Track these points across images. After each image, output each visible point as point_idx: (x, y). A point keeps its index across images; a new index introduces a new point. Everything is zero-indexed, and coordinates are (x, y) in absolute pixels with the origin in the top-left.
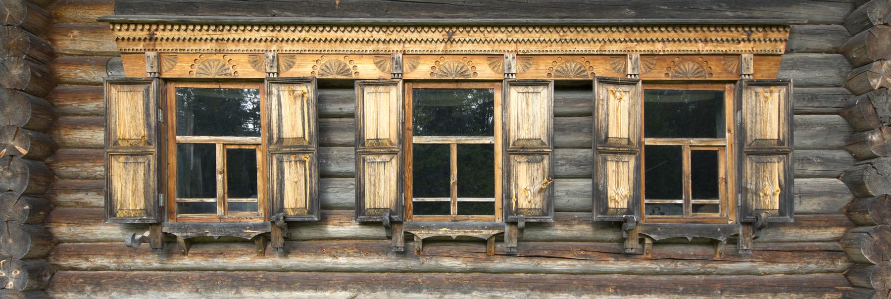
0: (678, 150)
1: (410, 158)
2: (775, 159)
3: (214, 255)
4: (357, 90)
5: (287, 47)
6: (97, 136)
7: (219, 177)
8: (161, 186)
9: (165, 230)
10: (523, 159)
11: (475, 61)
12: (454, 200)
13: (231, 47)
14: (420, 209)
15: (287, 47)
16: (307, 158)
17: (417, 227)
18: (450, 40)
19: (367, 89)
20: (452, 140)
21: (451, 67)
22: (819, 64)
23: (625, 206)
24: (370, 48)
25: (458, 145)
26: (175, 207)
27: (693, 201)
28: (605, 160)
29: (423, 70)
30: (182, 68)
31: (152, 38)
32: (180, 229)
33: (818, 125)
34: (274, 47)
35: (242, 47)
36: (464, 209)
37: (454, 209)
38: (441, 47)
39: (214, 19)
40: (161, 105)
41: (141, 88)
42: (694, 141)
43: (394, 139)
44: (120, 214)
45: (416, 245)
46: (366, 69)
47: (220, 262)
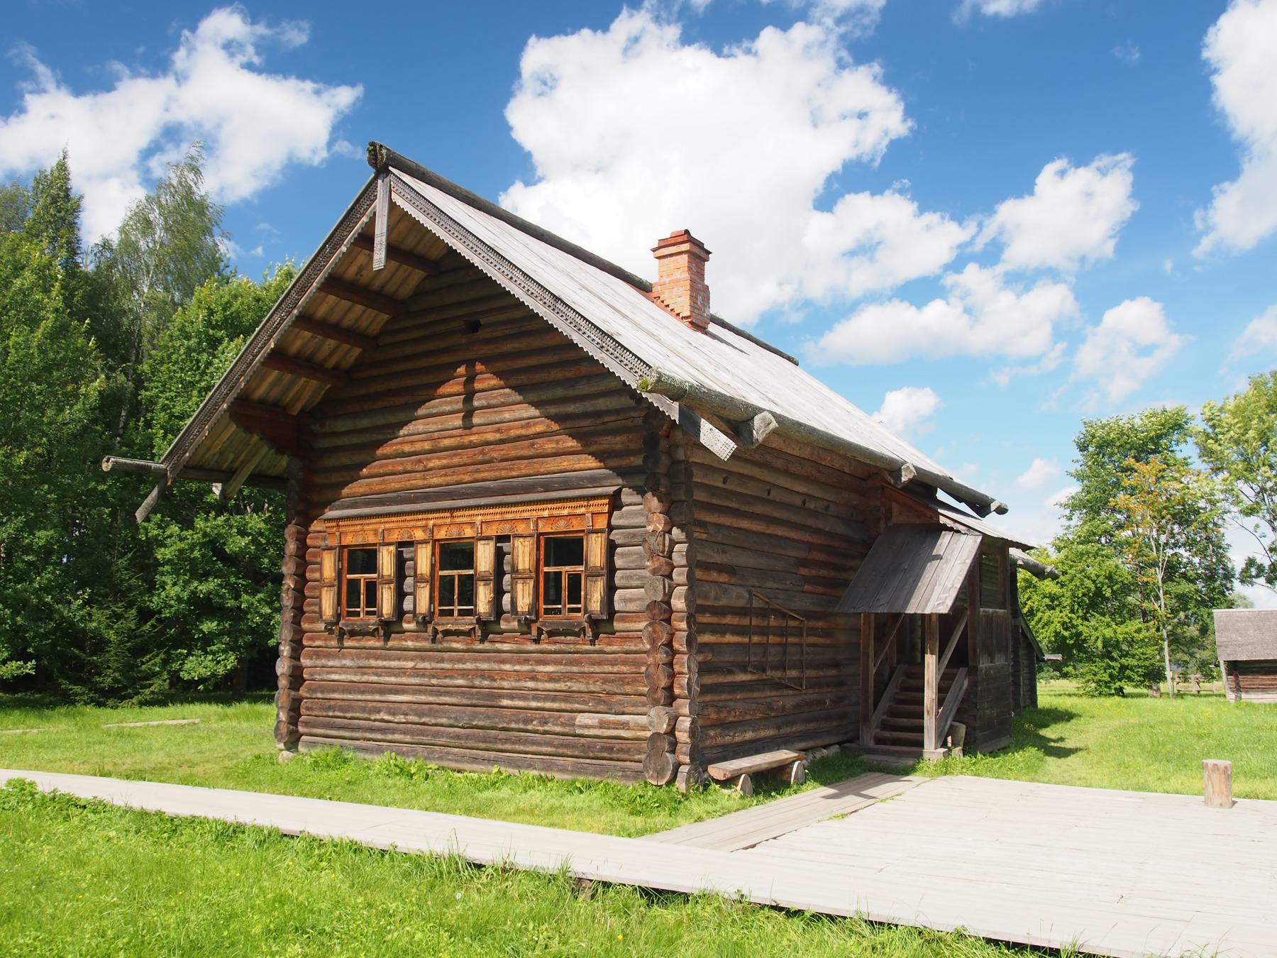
0: (358, 581)
1: (437, 584)
2: (599, 578)
3: (359, 640)
4: (415, 545)
5: (388, 526)
6: (317, 575)
7: (362, 596)
8: (339, 603)
9: (340, 626)
10: (482, 583)
11: (464, 526)
12: (456, 608)
13: (366, 527)
14: (442, 613)
15: (388, 526)
16: (392, 586)
17: (438, 624)
18: (452, 517)
19: (419, 546)
20: (455, 572)
21: (454, 532)
22: (636, 514)
23: (527, 610)
24: (420, 523)
25: (459, 576)
26: (345, 613)
27: (568, 606)
28: (517, 583)
29: (441, 534)
30: (348, 540)
31: (338, 526)
32: (346, 626)
33: (635, 554)
34: (382, 526)
35: (371, 527)
36: (462, 613)
37: (456, 613)
38: (448, 521)
39: (350, 792)
40: (340, 559)
41: (333, 551)
42: (567, 568)
43: (428, 574)
44: (324, 618)
45: (439, 636)
46: (419, 535)
47: (362, 643)
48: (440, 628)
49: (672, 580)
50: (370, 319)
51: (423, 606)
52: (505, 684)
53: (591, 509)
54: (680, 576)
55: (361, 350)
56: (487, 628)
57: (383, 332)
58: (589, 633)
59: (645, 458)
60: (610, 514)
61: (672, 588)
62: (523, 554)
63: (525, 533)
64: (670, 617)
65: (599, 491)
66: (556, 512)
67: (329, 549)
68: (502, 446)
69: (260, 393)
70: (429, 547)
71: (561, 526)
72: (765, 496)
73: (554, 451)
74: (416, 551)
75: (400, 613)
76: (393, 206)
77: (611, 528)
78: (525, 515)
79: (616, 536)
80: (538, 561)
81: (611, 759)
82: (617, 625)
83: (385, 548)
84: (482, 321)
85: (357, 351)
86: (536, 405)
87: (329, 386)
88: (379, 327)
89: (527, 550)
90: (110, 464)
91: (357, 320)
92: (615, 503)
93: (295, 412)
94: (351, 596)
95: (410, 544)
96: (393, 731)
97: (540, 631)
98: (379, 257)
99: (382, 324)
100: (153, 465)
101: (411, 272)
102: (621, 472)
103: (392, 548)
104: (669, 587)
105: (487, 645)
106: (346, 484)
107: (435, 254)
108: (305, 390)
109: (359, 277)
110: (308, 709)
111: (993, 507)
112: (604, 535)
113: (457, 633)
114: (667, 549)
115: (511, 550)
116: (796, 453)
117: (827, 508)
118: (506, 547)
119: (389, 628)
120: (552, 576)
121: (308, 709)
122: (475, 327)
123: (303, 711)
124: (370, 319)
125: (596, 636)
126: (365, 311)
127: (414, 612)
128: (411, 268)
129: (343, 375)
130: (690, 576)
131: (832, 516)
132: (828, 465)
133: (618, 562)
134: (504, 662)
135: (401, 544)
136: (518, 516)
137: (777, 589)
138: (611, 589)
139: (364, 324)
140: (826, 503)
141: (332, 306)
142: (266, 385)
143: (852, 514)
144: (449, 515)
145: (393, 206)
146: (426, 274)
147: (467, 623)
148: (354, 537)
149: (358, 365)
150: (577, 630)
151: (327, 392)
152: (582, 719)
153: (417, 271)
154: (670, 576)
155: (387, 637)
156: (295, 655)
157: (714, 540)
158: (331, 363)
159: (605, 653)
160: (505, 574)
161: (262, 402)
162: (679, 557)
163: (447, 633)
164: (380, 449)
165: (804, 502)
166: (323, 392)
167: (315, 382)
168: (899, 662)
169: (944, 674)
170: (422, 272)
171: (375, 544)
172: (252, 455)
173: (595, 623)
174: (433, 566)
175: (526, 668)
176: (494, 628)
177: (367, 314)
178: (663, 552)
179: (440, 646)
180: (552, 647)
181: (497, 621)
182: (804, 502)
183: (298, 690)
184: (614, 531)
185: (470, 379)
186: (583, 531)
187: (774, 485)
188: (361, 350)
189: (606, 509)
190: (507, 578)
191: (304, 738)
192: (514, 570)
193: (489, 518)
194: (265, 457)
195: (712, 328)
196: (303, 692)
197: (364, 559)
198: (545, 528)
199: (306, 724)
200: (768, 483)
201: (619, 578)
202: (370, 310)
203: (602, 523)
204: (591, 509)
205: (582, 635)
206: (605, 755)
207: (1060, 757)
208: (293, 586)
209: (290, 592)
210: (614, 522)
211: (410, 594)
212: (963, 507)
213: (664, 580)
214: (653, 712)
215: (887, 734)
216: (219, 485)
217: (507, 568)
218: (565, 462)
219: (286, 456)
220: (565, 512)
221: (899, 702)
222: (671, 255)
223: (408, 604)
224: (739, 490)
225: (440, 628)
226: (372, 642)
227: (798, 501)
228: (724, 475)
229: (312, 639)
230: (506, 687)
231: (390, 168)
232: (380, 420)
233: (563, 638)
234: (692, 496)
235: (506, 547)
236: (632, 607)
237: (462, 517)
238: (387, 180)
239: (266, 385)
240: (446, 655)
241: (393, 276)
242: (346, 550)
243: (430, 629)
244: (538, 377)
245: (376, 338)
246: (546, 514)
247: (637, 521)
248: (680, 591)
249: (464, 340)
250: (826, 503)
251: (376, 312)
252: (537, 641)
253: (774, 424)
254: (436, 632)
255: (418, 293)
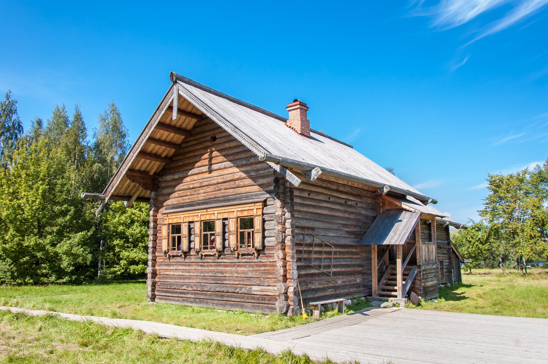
6: (160, 235)
30: (171, 221)
31: (168, 216)
38: (206, 213)
40: (169, 229)
45: (203, 257)
46: (196, 219)
48: (203, 254)
49: (285, 233)
50: (178, 138)
51: (197, 247)
52: (227, 275)
53: (256, 207)
54: (288, 232)
55: (175, 150)
56: (186, 254)
57: (183, 142)
58: (256, 255)
59: (275, 187)
60: (263, 209)
61: (285, 237)
62: (232, 226)
63: (232, 217)
64: (285, 248)
65: (259, 200)
66: (243, 209)
67: (165, 225)
68: (224, 184)
69: (137, 168)
70: (199, 223)
71: (245, 214)
72: (328, 200)
73: (243, 185)
74: (194, 225)
75: (190, 249)
76: (180, 96)
77: (263, 214)
78: (232, 210)
79: (266, 217)
80: (237, 227)
81: (265, 304)
82: (266, 252)
83: (184, 224)
84: (217, 137)
85: (173, 150)
86: (238, 167)
87: (164, 164)
88: (181, 141)
89: (234, 223)
90: (84, 195)
91: (173, 138)
92: (265, 203)
93: (152, 173)
94: (176, 242)
95: (192, 222)
96: (188, 293)
97: (238, 254)
98: (175, 115)
99: (182, 140)
100: (100, 195)
101: (191, 120)
102: (269, 192)
103: (187, 224)
104: (284, 236)
105: (220, 260)
106: (166, 201)
107: (198, 113)
108: (154, 166)
109: (171, 122)
110: (158, 286)
111: (430, 201)
112: (261, 217)
113: (210, 255)
114: (283, 222)
115: (228, 224)
116: (341, 182)
117: (357, 204)
118: (226, 222)
119: (186, 254)
120: (422, 231)
121: (158, 286)
122: (214, 139)
123: (156, 286)
124: (178, 138)
125: (259, 255)
126: (175, 135)
127: (194, 248)
128: (191, 118)
129: (169, 159)
130: (292, 232)
131: (359, 207)
132: (356, 186)
133: (266, 227)
134: (226, 266)
135: (190, 222)
136: (230, 210)
137: (334, 236)
138: (264, 237)
139: (175, 140)
140: (356, 202)
141: (165, 135)
142: (140, 164)
143: (368, 206)
144: (206, 211)
145: (180, 96)
146: (197, 120)
147: (180, 253)
148: (175, 219)
149: (174, 155)
150: (252, 253)
151: (164, 165)
152: (254, 288)
153: (193, 119)
154: (285, 232)
155: (185, 257)
156: (153, 266)
157: (305, 217)
158: (164, 155)
159: (262, 262)
160: (226, 233)
161: (139, 171)
162: (288, 225)
163: (206, 255)
164: (177, 187)
165: (346, 202)
166: (162, 166)
167: (159, 162)
168: (390, 264)
169: (405, 268)
170: (195, 120)
171: (180, 223)
172: (137, 190)
173: (258, 251)
174: (201, 230)
175: (234, 269)
176: (188, 254)
177: (176, 136)
178: (282, 222)
179: (204, 261)
180: (244, 261)
181: (223, 251)
182: (346, 202)
183: (155, 278)
184: (265, 215)
185: (211, 159)
186: (253, 215)
187: (332, 195)
188: (175, 150)
189: (261, 207)
190: (227, 234)
191: (157, 296)
192: (229, 231)
193: (220, 212)
194: (141, 191)
195: (312, 134)
196: (157, 280)
197: (176, 229)
198: (240, 214)
199: (158, 291)
200: (329, 195)
201: (266, 233)
202: (177, 135)
203: (260, 212)
204: (256, 207)
205: (254, 256)
206: (263, 302)
207: (459, 301)
208: (152, 239)
209: (151, 242)
210: (265, 212)
211: (193, 241)
212: (418, 202)
213: (282, 234)
214: (278, 285)
215: (384, 293)
216: (126, 202)
217: (227, 230)
218: (247, 189)
219: (149, 190)
220: (247, 208)
221: (389, 280)
222: (294, 109)
223: (192, 246)
224: (315, 198)
225: (203, 254)
226: (179, 259)
227: (343, 202)
228: (309, 193)
229: (160, 259)
230: (227, 276)
231: (178, 81)
232: (176, 177)
233: (247, 257)
234: (293, 200)
235: (226, 222)
236: (271, 244)
237: (210, 211)
238: (177, 85)
239: (140, 164)
240: (206, 264)
241: (184, 122)
242: (171, 225)
243: (200, 254)
244: (237, 157)
245: (180, 145)
246: (240, 209)
247: (273, 211)
248: (289, 238)
249: (210, 144)
250: (356, 202)
251: (179, 135)
252: (238, 258)
253: (320, 172)
254: (202, 255)
255: (195, 127)
